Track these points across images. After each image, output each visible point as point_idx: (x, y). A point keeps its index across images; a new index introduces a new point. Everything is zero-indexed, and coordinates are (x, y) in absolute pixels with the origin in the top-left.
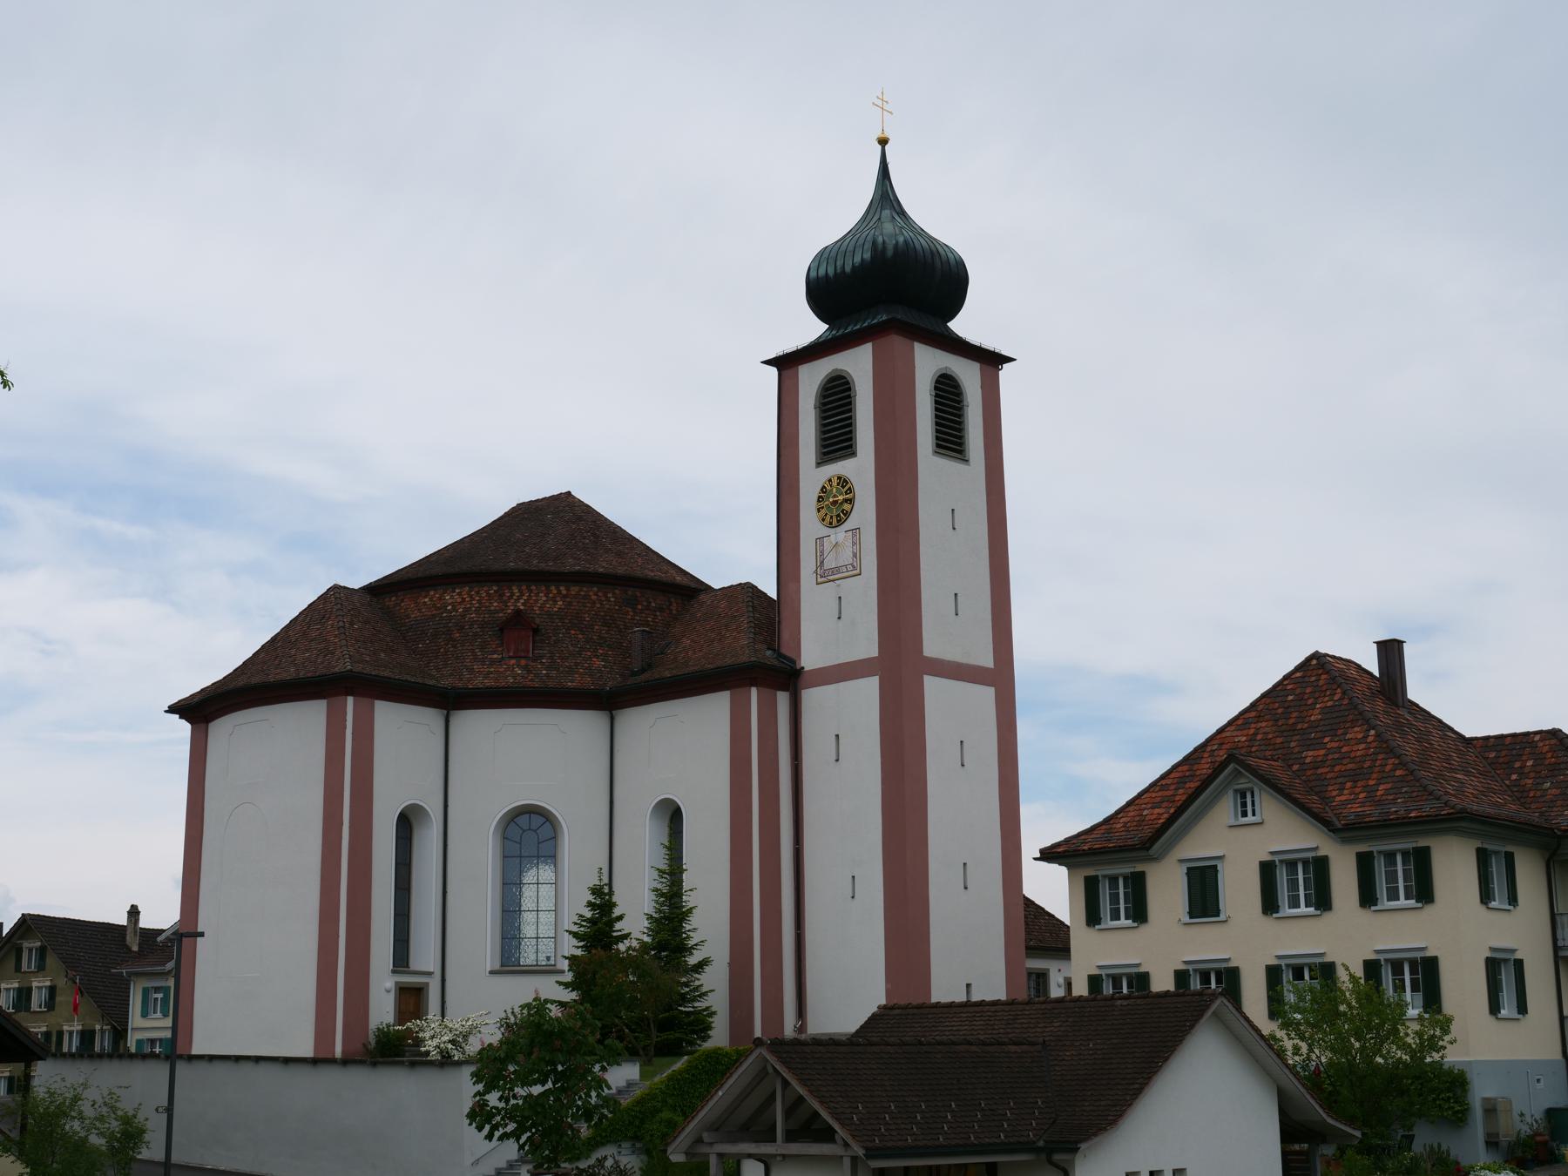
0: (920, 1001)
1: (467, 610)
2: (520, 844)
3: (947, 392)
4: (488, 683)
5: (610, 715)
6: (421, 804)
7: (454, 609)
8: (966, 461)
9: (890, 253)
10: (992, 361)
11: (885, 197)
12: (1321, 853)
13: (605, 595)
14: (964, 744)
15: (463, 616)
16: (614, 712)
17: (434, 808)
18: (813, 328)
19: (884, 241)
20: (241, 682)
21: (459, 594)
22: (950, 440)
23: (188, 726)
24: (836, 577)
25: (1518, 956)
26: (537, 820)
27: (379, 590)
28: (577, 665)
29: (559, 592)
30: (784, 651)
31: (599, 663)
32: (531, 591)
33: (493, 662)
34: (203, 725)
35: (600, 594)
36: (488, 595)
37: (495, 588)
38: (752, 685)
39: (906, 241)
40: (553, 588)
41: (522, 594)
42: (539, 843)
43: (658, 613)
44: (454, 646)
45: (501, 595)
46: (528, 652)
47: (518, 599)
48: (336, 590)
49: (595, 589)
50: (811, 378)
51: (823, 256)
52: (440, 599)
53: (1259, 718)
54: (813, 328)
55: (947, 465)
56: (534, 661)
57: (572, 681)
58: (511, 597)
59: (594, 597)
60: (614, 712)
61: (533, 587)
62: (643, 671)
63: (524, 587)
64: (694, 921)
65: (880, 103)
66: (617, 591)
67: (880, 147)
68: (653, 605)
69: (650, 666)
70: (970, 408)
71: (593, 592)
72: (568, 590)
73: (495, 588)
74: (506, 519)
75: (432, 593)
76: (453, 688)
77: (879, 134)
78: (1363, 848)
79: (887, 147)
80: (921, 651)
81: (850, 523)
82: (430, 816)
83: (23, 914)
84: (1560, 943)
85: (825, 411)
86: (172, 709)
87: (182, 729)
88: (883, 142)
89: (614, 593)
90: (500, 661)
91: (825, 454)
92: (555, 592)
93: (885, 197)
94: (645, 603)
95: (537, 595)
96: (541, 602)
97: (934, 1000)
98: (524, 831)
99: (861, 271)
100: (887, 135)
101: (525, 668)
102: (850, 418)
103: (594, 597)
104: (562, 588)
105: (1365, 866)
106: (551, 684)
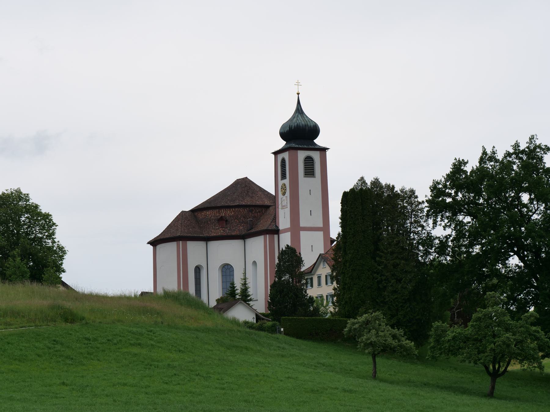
1: (211, 216)
2: (226, 272)
3: (309, 161)
4: (215, 235)
5: (244, 241)
6: (201, 264)
7: (209, 216)
9: (293, 128)
10: (323, 150)
11: (299, 110)
14: (313, 246)
16: (245, 240)
17: (204, 265)
18: (282, 143)
19: (292, 125)
20: (159, 238)
21: (210, 212)
22: (309, 171)
23: (152, 247)
24: (284, 208)
26: (226, 267)
28: (236, 229)
30: (277, 225)
31: (241, 228)
32: (226, 210)
33: (216, 229)
34: (155, 247)
35: (243, 210)
36: (216, 212)
37: (218, 210)
38: (267, 234)
39: (297, 125)
40: (231, 209)
41: (224, 212)
43: (258, 213)
44: (208, 225)
45: (219, 212)
46: (224, 226)
47: (223, 213)
48: (183, 212)
49: (242, 209)
50: (280, 157)
51: (283, 127)
52: (206, 213)
55: (310, 180)
56: (226, 228)
57: (234, 233)
58: (221, 212)
59: (241, 211)
60: (245, 240)
61: (227, 209)
62: (250, 229)
63: (224, 210)
64: (249, 290)
65: (297, 84)
66: (247, 209)
67: (297, 95)
68: (257, 211)
69: (252, 228)
70: (316, 164)
71: (241, 210)
72: (235, 209)
73: (218, 210)
75: (204, 212)
77: (297, 92)
79: (299, 95)
80: (300, 226)
81: (286, 195)
82: (203, 267)
83: (142, 292)
85: (282, 167)
86: (148, 243)
87: (151, 248)
88: (298, 94)
89: (247, 209)
91: (283, 177)
92: (232, 210)
93: (299, 110)
94: (255, 211)
95: (227, 211)
96: (228, 213)
100: (300, 92)
101: (224, 231)
102: (285, 169)
103: (241, 211)
104: (233, 209)
106: (229, 234)
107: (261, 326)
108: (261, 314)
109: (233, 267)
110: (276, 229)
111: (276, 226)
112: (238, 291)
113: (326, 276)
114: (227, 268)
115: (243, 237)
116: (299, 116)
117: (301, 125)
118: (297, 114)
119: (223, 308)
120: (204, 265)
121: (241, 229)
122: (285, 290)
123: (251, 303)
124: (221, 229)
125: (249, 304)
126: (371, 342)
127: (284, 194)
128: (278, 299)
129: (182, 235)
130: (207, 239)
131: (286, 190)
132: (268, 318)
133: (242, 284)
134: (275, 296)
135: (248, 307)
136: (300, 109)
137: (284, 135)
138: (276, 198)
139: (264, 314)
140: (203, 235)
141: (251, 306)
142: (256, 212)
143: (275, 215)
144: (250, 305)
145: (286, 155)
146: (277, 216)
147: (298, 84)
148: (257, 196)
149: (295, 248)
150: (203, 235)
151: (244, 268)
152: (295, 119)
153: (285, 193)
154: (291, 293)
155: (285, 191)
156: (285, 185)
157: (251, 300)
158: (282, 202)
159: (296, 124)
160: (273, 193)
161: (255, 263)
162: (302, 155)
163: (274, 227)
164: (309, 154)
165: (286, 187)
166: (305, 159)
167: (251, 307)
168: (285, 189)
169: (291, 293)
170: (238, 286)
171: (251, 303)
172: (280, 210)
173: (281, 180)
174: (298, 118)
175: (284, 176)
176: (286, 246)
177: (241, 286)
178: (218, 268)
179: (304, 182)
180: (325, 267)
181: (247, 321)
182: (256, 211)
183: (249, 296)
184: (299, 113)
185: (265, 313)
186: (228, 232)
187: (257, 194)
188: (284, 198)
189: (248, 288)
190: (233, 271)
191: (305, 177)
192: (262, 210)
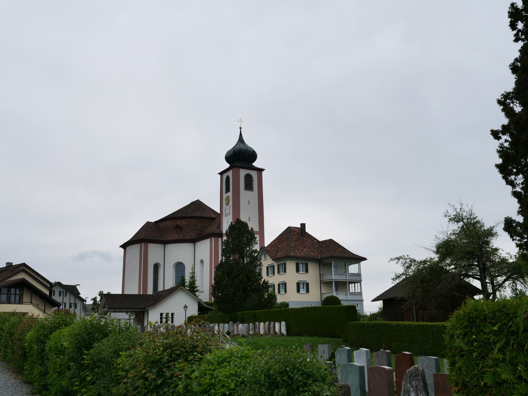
0: (146, 294)
1: (169, 225)
3: (248, 178)
4: (171, 239)
8: (253, 191)
9: (236, 151)
10: (260, 170)
11: (241, 140)
12: (274, 264)
13: (195, 220)
15: (169, 226)
18: (227, 165)
20: (133, 239)
22: (249, 186)
23: (123, 249)
25: (307, 282)
26: (179, 265)
27: (156, 222)
28: (188, 234)
29: (186, 220)
30: (221, 230)
31: (192, 234)
39: (240, 149)
42: (182, 269)
47: (179, 222)
50: (225, 176)
53: (310, 238)
54: (227, 165)
55: (249, 193)
64: (196, 282)
70: (254, 181)
74: (203, 205)
76: (165, 240)
77: (240, 127)
78: (278, 263)
82: (161, 265)
84: (321, 280)
86: (120, 247)
87: (122, 250)
88: (241, 128)
90: (174, 235)
93: (241, 140)
97: (124, 294)
98: (179, 267)
99: (232, 155)
100: (241, 127)
101: (178, 236)
105: (278, 266)
106: (182, 238)
107: (160, 374)
108: (205, 303)
109: (184, 265)
110: (220, 233)
111: (220, 231)
112: (187, 284)
113: (267, 267)
114: (180, 266)
115: (194, 241)
116: (241, 144)
117: (243, 149)
118: (240, 142)
119: (162, 295)
120: (162, 263)
121: (193, 235)
122: (234, 271)
123: (197, 293)
124: (176, 234)
125: (195, 295)
126: (477, 379)
127: (227, 204)
128: (225, 282)
129: (144, 238)
130: (165, 243)
131: (229, 201)
132: (212, 307)
133: (191, 277)
134: (221, 278)
135: (190, 294)
136: (241, 139)
137: (228, 159)
138: (221, 216)
139: (208, 302)
140: (162, 239)
141: (198, 296)
142: (204, 222)
143: (220, 222)
144: (197, 295)
145: (230, 173)
146: (221, 223)
147: (240, 121)
148: (206, 212)
149: (246, 223)
150: (162, 239)
151: (193, 264)
152: (238, 146)
153: (229, 203)
154: (242, 275)
155: (229, 201)
156: (228, 197)
157: (197, 291)
158: (225, 211)
159: (239, 148)
160: (218, 211)
161: (202, 261)
162: (243, 173)
163: (219, 232)
164: (249, 172)
165: (229, 198)
166: (246, 176)
167: (197, 297)
168: (229, 200)
169: (242, 275)
170: (187, 279)
171: (197, 293)
172: (224, 216)
173: (226, 193)
174: (241, 145)
175: (228, 190)
176: (236, 220)
177: (190, 279)
178: (173, 264)
179: (245, 195)
180: (266, 259)
181: (504, 225)
182: (205, 221)
183: (196, 287)
184: (241, 142)
185: (208, 301)
186: (181, 237)
187: (206, 210)
188: (228, 207)
189: (196, 281)
190: (185, 268)
191: (245, 190)
192: (210, 221)
